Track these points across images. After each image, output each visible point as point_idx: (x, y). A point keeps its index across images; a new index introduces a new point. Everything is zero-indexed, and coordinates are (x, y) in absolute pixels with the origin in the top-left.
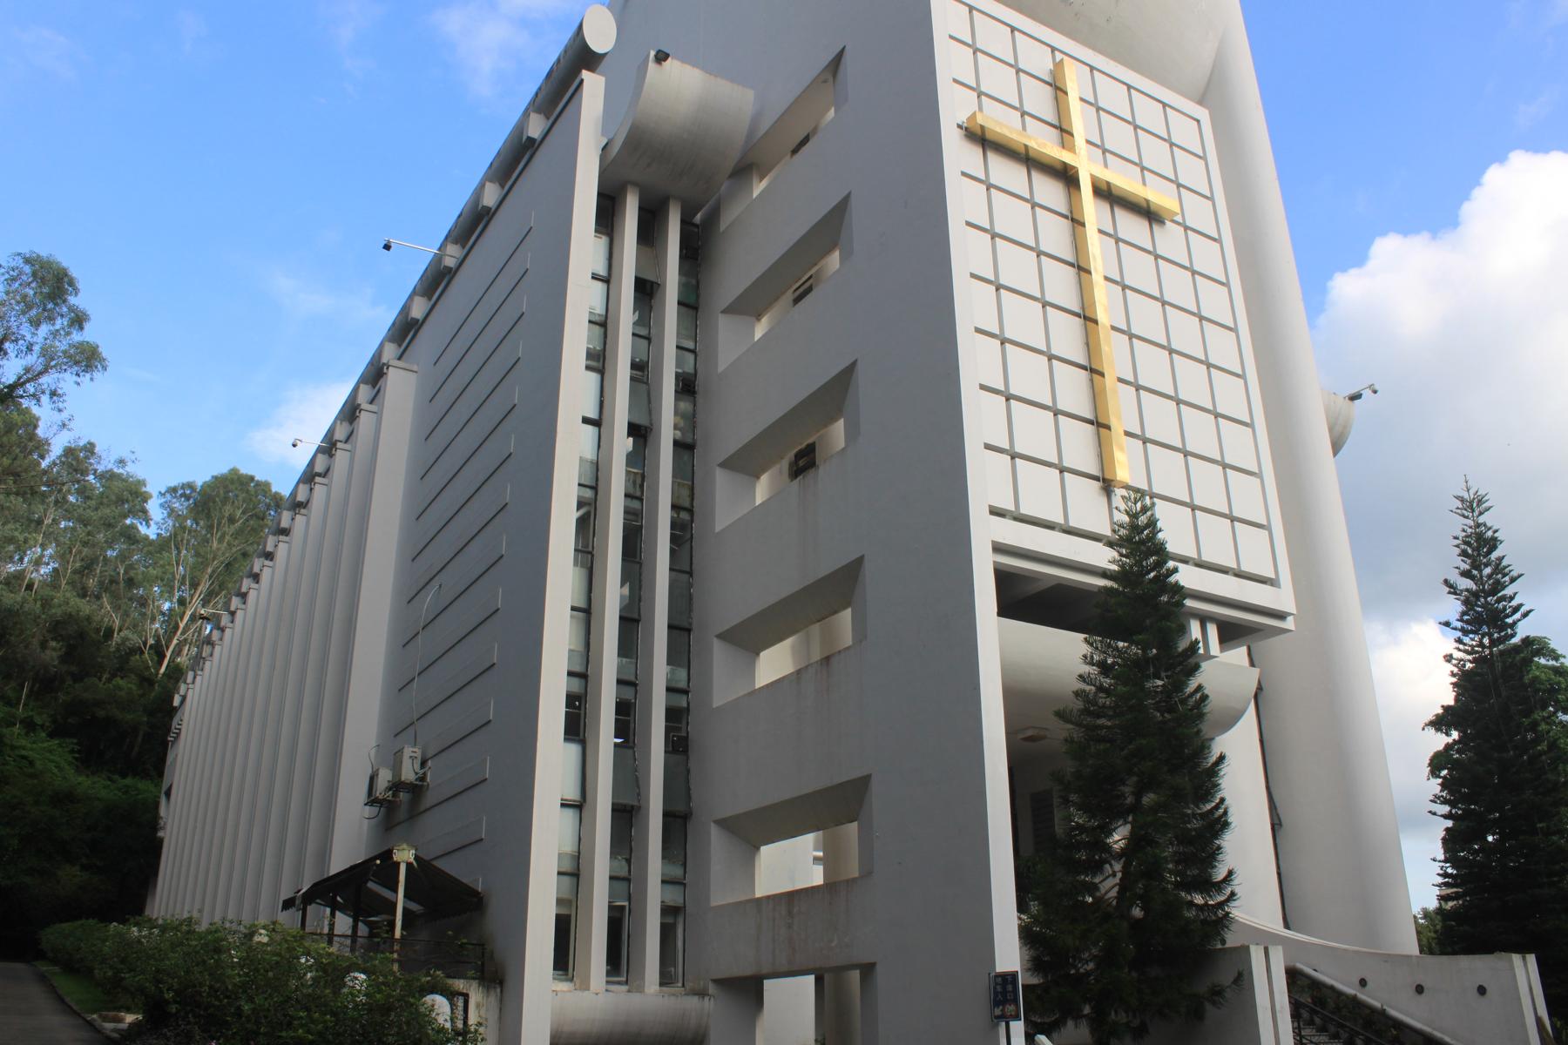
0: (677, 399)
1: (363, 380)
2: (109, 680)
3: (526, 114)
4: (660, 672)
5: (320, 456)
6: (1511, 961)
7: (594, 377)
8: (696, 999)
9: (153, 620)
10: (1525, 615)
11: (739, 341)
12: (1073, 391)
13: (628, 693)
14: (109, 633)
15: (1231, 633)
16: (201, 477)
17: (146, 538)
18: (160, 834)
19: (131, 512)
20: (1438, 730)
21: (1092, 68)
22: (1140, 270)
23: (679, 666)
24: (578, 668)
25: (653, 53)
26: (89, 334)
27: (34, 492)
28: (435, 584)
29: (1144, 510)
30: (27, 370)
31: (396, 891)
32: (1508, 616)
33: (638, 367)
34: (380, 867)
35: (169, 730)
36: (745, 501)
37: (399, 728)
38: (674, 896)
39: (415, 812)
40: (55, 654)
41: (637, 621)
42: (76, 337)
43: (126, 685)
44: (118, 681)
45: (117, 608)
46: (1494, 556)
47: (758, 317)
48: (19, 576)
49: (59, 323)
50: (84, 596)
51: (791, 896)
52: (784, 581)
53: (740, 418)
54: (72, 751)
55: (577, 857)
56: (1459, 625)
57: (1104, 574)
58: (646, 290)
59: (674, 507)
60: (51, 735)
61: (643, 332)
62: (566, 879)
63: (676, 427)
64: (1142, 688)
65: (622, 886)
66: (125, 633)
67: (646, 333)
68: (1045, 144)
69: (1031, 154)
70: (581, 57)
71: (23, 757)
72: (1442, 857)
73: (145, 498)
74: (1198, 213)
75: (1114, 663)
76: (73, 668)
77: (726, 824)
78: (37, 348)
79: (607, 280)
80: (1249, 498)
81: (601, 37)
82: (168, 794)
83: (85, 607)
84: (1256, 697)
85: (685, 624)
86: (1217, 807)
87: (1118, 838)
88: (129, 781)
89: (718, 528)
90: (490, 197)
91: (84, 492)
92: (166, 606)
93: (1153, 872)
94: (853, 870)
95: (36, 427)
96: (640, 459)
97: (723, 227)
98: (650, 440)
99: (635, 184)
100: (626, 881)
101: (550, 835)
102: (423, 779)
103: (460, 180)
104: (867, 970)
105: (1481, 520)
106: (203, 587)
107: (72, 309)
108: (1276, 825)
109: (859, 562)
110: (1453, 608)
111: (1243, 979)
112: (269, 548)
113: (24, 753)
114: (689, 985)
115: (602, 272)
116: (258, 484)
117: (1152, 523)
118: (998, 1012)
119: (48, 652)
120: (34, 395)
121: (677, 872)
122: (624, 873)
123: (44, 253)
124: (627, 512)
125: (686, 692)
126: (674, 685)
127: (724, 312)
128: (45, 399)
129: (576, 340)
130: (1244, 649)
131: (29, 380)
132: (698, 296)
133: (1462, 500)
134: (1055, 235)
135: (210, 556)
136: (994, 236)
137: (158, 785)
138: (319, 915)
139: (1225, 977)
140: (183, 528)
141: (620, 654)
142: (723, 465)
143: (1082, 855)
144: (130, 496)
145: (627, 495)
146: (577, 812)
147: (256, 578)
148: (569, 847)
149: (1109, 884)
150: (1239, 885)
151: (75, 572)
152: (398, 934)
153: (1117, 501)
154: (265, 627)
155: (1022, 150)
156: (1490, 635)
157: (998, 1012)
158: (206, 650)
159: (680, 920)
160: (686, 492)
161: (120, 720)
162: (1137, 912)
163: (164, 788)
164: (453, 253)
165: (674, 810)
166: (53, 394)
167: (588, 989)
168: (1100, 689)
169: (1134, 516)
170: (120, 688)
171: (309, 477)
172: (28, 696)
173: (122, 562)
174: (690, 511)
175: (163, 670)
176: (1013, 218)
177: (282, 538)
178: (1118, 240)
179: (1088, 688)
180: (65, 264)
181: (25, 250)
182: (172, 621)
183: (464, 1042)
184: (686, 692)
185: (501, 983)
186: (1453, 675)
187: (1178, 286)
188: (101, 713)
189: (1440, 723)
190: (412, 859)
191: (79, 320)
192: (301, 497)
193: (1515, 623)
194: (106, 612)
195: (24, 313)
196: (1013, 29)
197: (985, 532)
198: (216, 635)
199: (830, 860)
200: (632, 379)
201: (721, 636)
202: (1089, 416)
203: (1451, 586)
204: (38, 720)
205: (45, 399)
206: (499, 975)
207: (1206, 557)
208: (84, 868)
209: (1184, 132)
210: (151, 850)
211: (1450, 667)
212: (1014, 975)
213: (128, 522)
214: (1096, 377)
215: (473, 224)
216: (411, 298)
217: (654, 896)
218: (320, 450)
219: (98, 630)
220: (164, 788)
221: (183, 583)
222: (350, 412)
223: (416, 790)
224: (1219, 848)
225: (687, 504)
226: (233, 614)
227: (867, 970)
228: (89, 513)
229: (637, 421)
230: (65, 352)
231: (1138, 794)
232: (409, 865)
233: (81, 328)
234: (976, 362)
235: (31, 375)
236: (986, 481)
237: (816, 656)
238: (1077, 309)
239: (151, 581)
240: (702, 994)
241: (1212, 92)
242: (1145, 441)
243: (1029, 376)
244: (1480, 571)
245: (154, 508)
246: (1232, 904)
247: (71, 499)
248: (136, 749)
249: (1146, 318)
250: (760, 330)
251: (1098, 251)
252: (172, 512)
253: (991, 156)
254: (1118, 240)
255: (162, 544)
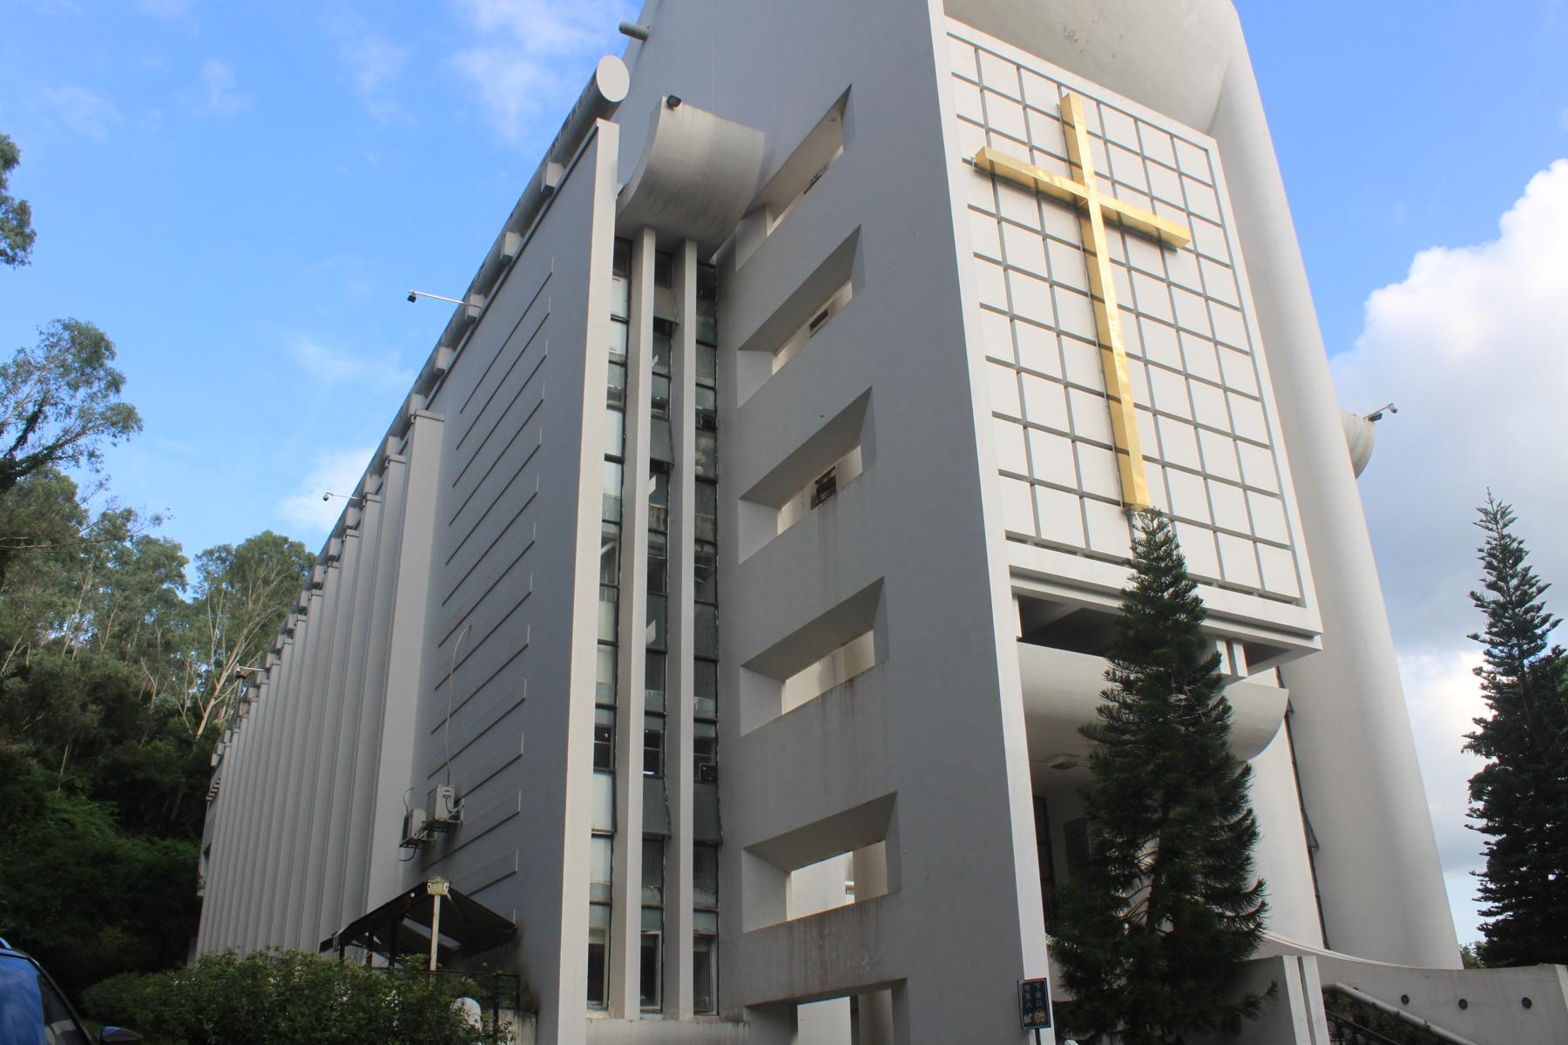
0: (697, 436)
1: (393, 432)
2: (148, 743)
3: (544, 164)
4: (688, 703)
5: (351, 510)
6: (1555, 971)
7: (615, 416)
8: (730, 1025)
9: (191, 683)
10: (1555, 625)
11: (755, 377)
12: (1090, 418)
13: (657, 724)
14: (147, 696)
15: (1258, 655)
16: (236, 540)
17: (183, 602)
18: (200, 893)
19: (168, 578)
20: (1478, 751)
21: (1099, 102)
22: (1152, 297)
23: (706, 696)
24: (606, 701)
25: (665, 99)
26: (126, 396)
27: (72, 558)
28: (466, 624)
29: (1161, 527)
30: (66, 432)
31: (430, 926)
32: (1537, 627)
33: (659, 405)
34: (414, 902)
35: (206, 790)
36: (767, 532)
37: (433, 770)
38: (707, 925)
39: (449, 852)
40: (96, 717)
41: (665, 653)
42: (113, 399)
43: (166, 746)
44: (157, 743)
45: (154, 671)
46: (1520, 567)
47: (776, 352)
48: (59, 642)
49: (96, 386)
50: (123, 659)
51: (822, 919)
52: (809, 607)
53: (758, 452)
54: (112, 814)
55: (610, 887)
56: (1488, 637)
57: (1123, 594)
58: (665, 330)
59: (698, 541)
60: (92, 798)
61: (664, 371)
62: (599, 909)
63: (697, 463)
64: (1165, 701)
65: (655, 915)
66: (162, 696)
67: (666, 373)
68: (1062, 183)
69: (1041, 187)
70: (596, 106)
71: (65, 820)
72: (1485, 870)
73: (182, 562)
74: (1209, 240)
75: (1138, 679)
76: (112, 731)
77: (756, 851)
78: (75, 411)
79: (626, 322)
80: (1271, 519)
81: (614, 86)
82: (207, 853)
83: (124, 669)
84: (1287, 717)
85: (711, 656)
86: (1245, 818)
87: (1146, 856)
88: (168, 842)
89: (741, 560)
90: (511, 247)
91: (122, 558)
92: (204, 668)
93: (1182, 883)
94: (883, 890)
95: (74, 494)
96: (663, 499)
97: (738, 266)
98: (672, 478)
99: (651, 227)
100: (658, 910)
101: (582, 867)
102: (456, 817)
103: (482, 229)
104: (898, 986)
105: (1505, 532)
106: (239, 649)
107: (110, 373)
108: (1313, 848)
109: (882, 579)
110: (1481, 622)
111: (1277, 990)
112: (303, 604)
113: (65, 816)
114: (724, 1013)
115: (622, 313)
116: (292, 545)
117: (1168, 540)
118: (1027, 1019)
119: (88, 714)
120: (73, 457)
121: (709, 900)
122: (656, 902)
123: (83, 320)
124: (651, 546)
125: (713, 722)
126: (702, 715)
127: (745, 347)
128: (83, 460)
129: (597, 380)
130: (1273, 671)
131: (66, 442)
132: (716, 335)
133: (1486, 512)
134: (1067, 266)
135: (246, 618)
136: (1007, 268)
137: (198, 846)
138: (356, 956)
139: (1260, 989)
140: (219, 590)
141: (647, 687)
142: (743, 498)
143: (1114, 871)
144: (166, 560)
145: (650, 531)
146: (608, 842)
147: (290, 633)
148: (601, 877)
149: (1139, 896)
150: (1270, 895)
151: (113, 637)
152: (433, 966)
153: (1138, 522)
154: (300, 680)
155: (1032, 184)
156: (1520, 646)
157: (1027, 1019)
158: (243, 708)
159: (714, 948)
160: (709, 526)
161: (157, 781)
162: (1167, 927)
163: (204, 847)
164: (477, 301)
165: (704, 839)
166: (91, 455)
167: (622, 1017)
168: (1124, 705)
169: (1151, 534)
170: (156, 749)
171: (340, 531)
172: (69, 760)
173: (160, 625)
174: (714, 544)
175: (200, 731)
176: (1025, 249)
177: (315, 591)
178: (1130, 269)
179: (1111, 704)
180: (101, 331)
181: (65, 317)
182: (209, 681)
183: (495, 1042)
184: (713, 722)
185: (536, 1013)
186: (1484, 688)
187: (1191, 312)
188: (140, 775)
189: (1479, 744)
190: (446, 892)
191: (115, 383)
192: (333, 552)
193: (1544, 633)
194: (146, 678)
195: (62, 376)
196: (1019, 67)
197: (1001, 558)
198: (252, 691)
199: (861, 873)
200: (653, 417)
201: (747, 666)
202: (1107, 442)
203: (1477, 599)
204: (79, 784)
205: (83, 460)
206: (529, 1000)
207: (1229, 579)
208: (126, 929)
209: (1192, 162)
210: (193, 908)
211: (1481, 680)
212: (1042, 982)
213: (165, 586)
214: (1112, 403)
215: (496, 273)
216: (436, 350)
217: (687, 925)
218: (351, 504)
219: (136, 694)
220: (204, 847)
221: (219, 646)
222: (380, 465)
223: (450, 828)
224: (1248, 858)
225: (710, 538)
226: (268, 670)
227: (898, 986)
228: (126, 578)
229: (658, 457)
230: (102, 414)
231: (1166, 807)
232: (443, 898)
233: (118, 391)
234: (989, 390)
235: (69, 437)
236: (1002, 507)
237: (842, 678)
238: (1091, 337)
239: (186, 643)
240: (737, 1020)
241: (1219, 122)
242: (1164, 465)
243: (1045, 403)
244: (1507, 583)
245: (191, 573)
246: (1263, 915)
247: (109, 565)
248: (176, 811)
249: (1161, 344)
250: (778, 363)
251: (1110, 279)
252: (208, 576)
253: (1002, 191)
254: (1130, 269)
255: (199, 608)
